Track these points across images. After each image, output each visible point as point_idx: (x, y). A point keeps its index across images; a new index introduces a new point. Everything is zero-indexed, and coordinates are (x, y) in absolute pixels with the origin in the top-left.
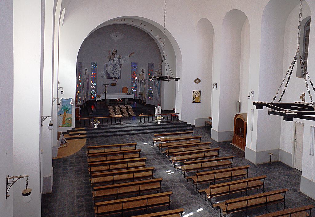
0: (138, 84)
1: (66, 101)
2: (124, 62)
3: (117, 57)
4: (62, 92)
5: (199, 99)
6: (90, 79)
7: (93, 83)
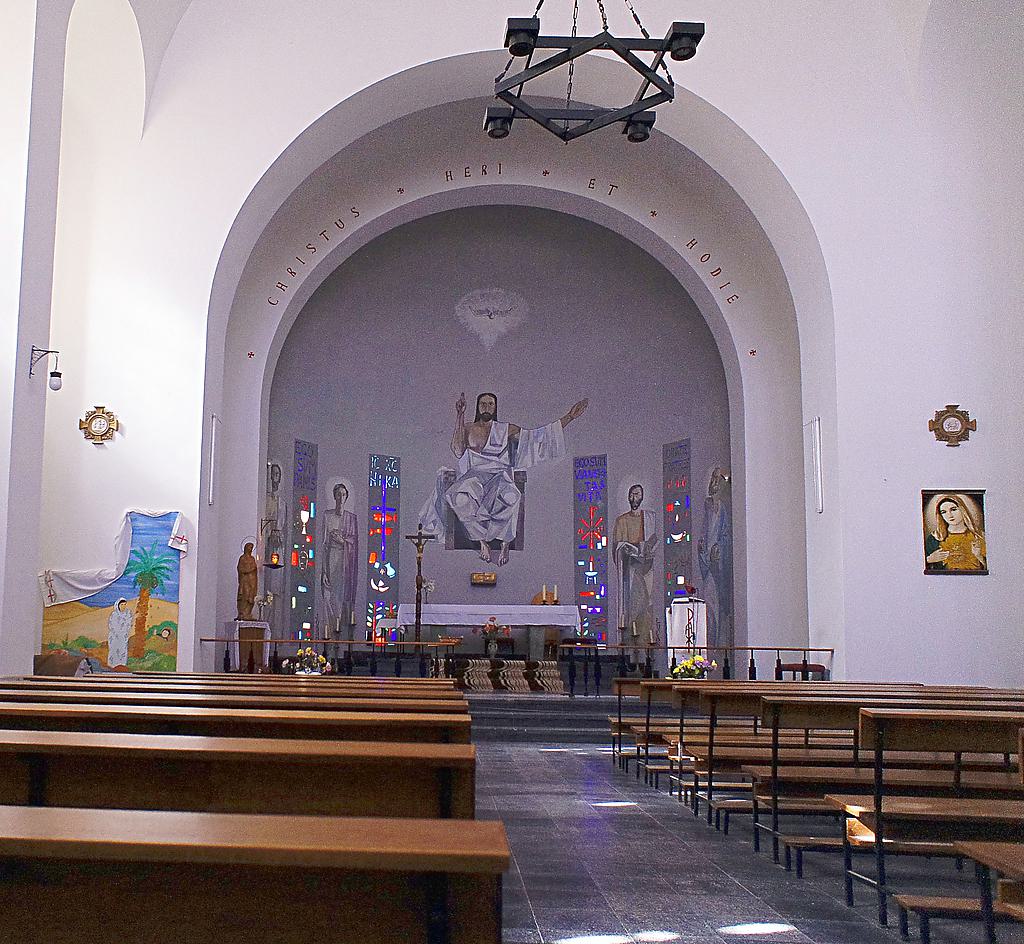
0: (614, 571)
1: (150, 524)
2: (537, 455)
3: (499, 433)
4: (53, 374)
5: (975, 551)
7: (377, 565)
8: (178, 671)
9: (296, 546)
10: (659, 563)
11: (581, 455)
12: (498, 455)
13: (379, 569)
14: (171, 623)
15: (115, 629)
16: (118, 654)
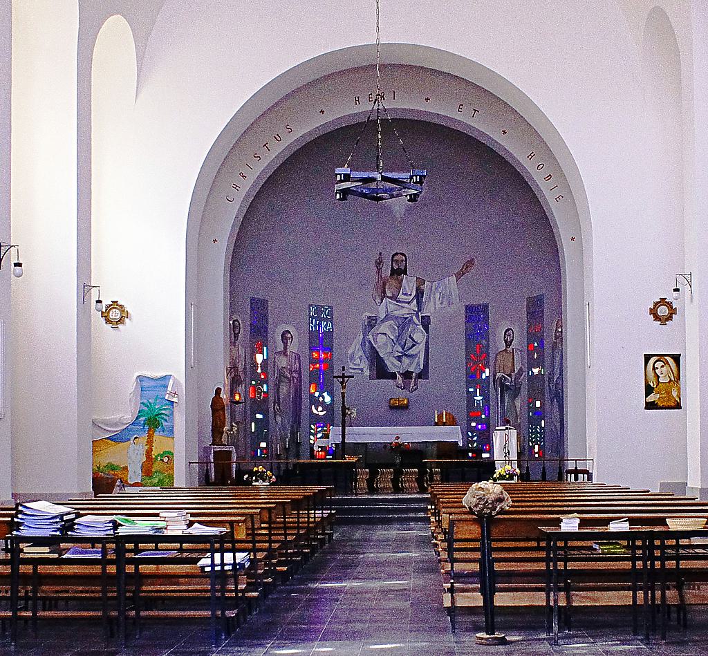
1: (152, 384)
2: (438, 303)
3: (409, 284)
5: (674, 394)
6: (306, 377)
7: (317, 394)
8: (175, 486)
9: (253, 382)
10: (524, 392)
11: (472, 302)
12: (409, 303)
13: (319, 397)
14: (169, 452)
15: (131, 457)
16: (135, 475)
